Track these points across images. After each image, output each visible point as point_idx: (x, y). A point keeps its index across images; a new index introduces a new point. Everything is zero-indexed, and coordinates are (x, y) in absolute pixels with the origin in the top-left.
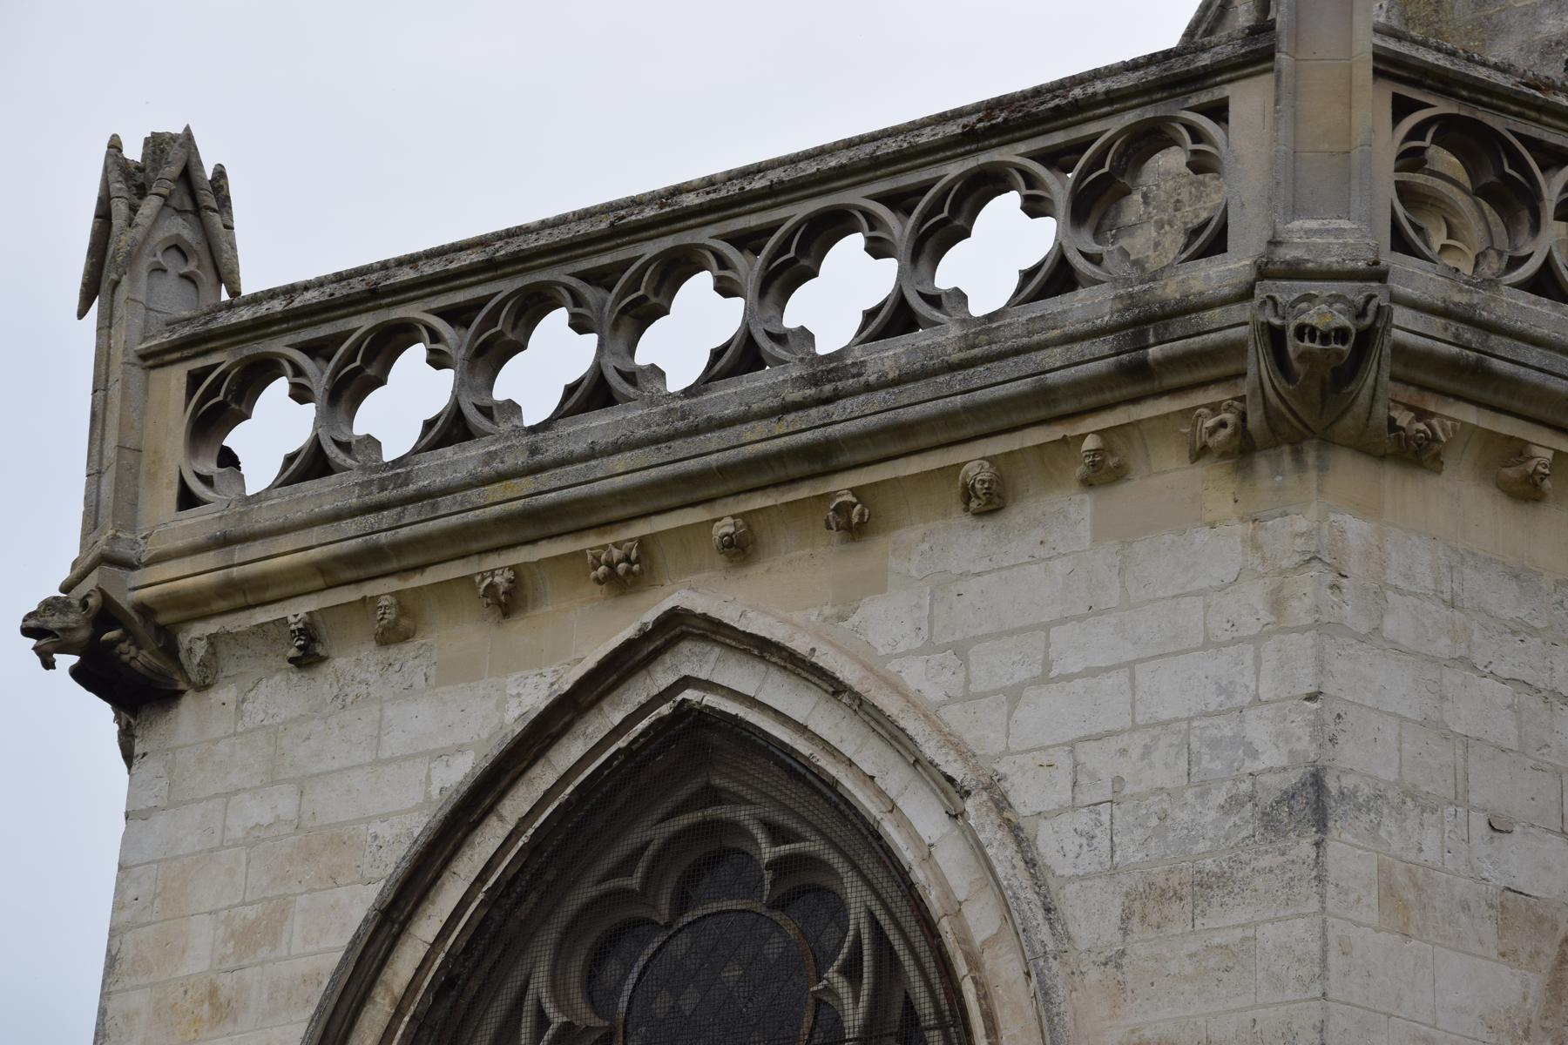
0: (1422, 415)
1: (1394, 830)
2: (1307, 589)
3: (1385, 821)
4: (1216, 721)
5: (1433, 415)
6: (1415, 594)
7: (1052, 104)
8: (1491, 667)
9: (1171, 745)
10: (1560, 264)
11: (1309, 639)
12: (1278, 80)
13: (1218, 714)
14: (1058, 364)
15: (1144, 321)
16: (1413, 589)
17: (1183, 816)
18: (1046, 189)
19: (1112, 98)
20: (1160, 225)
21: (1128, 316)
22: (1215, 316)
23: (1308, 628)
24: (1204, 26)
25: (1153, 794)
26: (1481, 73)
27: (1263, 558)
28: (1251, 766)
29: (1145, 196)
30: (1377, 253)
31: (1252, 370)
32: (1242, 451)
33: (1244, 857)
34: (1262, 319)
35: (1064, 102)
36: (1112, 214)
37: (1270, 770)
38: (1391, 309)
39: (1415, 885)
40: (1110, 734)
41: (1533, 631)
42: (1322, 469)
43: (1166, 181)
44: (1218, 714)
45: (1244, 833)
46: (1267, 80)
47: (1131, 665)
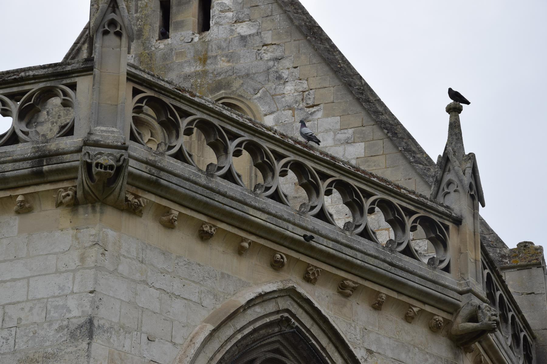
0: (137, 197)
1: (116, 339)
2: (93, 253)
3: (113, 336)
4: (57, 299)
5: (140, 197)
6: (130, 258)
7: (13, 77)
8: (153, 284)
9: (40, 307)
10: (184, 150)
11: (93, 272)
12: (94, 78)
13: (58, 297)
14: (10, 169)
15: (42, 156)
16: (130, 256)
17: (42, 333)
18: (9, 107)
19: (35, 77)
20: (53, 123)
21: (37, 154)
22: (68, 157)
23: (93, 268)
24: (71, 56)
25: (32, 324)
26: (162, 83)
27: (79, 242)
28: (68, 315)
29: (48, 112)
30: (125, 140)
31: (80, 177)
32: (74, 205)
33: (63, 348)
34: (84, 159)
35: (18, 77)
36: (35, 117)
37: (75, 317)
38: (128, 160)
39: (121, 359)
40: (19, 302)
41: (168, 273)
42: (102, 213)
43: (55, 108)
44: (58, 297)
45: (63, 339)
46: (90, 78)
47: (28, 278)
